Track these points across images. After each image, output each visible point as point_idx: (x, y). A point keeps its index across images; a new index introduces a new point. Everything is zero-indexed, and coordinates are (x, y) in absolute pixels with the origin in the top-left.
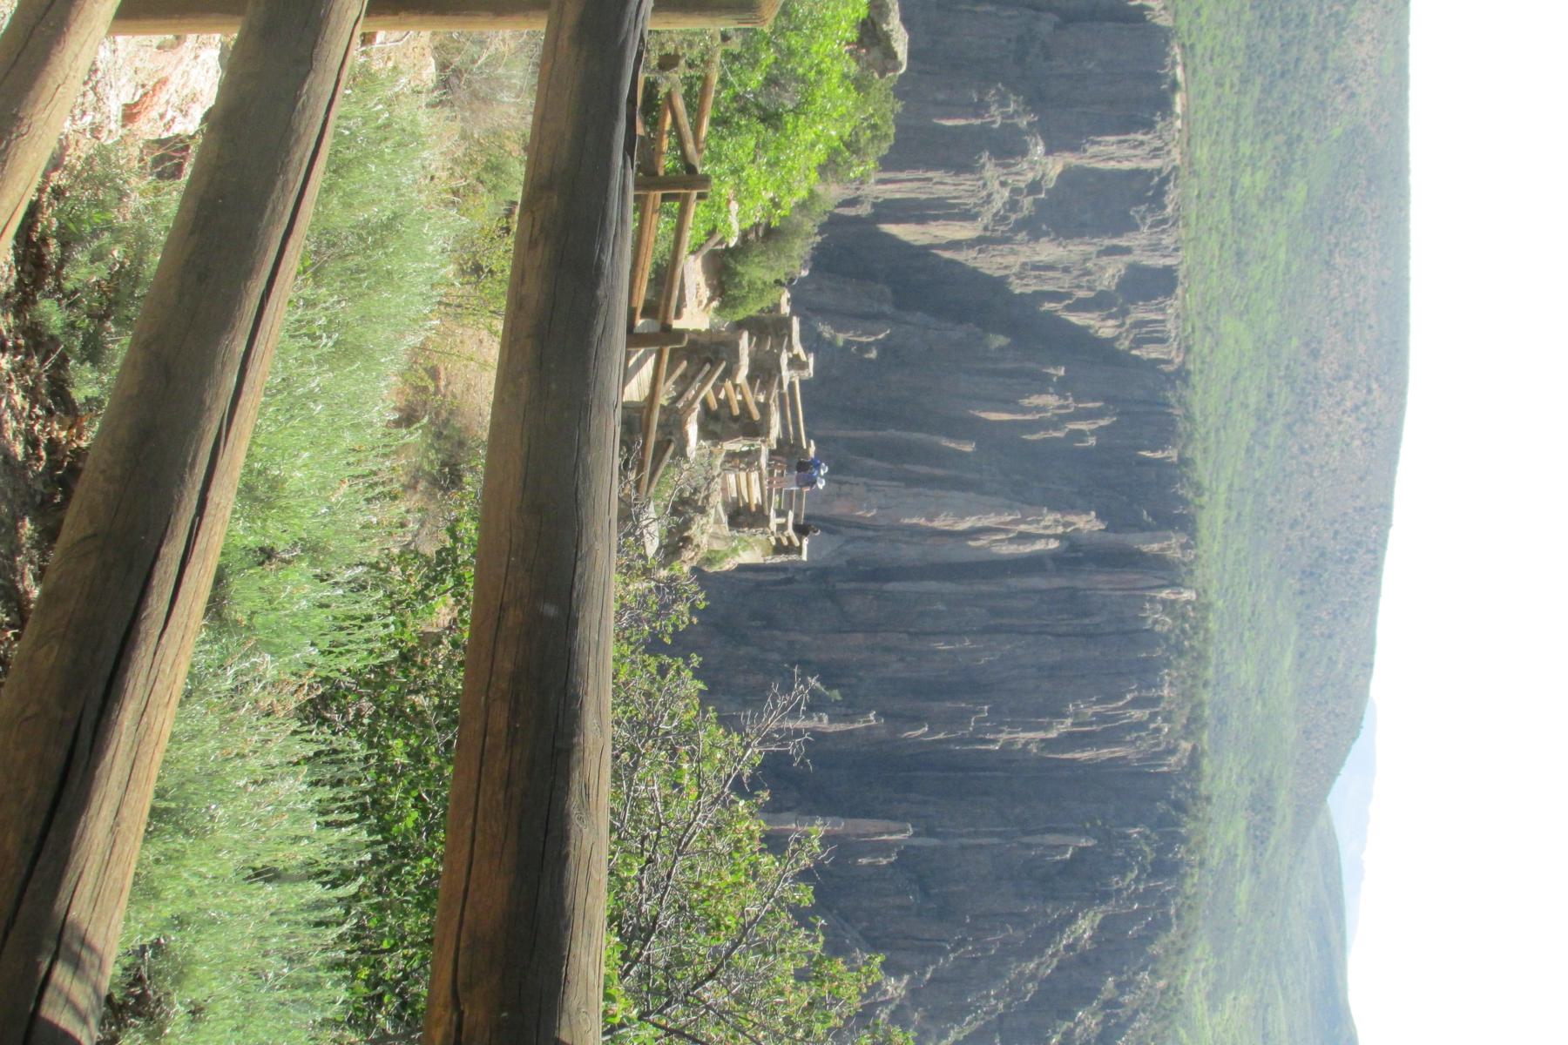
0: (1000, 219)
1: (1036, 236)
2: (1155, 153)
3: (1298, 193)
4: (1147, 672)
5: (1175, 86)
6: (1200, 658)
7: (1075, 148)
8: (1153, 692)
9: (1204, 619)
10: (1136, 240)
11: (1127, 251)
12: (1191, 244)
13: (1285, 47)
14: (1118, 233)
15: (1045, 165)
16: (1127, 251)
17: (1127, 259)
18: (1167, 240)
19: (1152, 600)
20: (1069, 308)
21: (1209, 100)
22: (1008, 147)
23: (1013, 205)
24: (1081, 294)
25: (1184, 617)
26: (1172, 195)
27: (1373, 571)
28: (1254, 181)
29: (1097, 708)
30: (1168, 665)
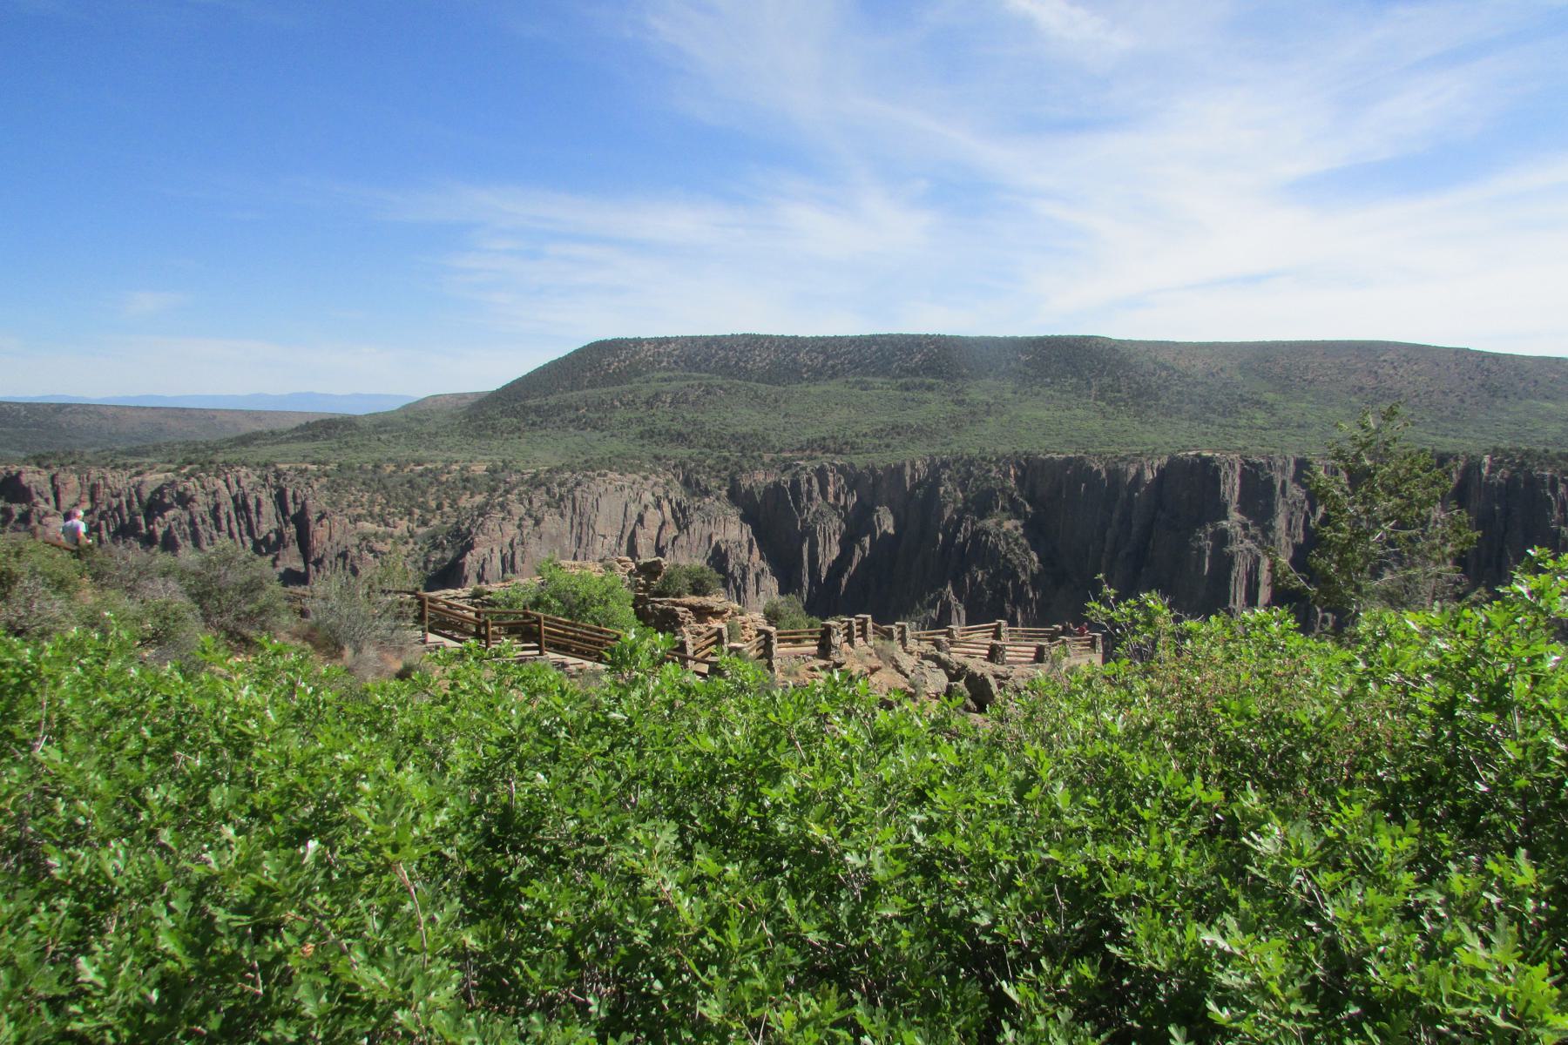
0: (1261, 545)
1: (1271, 528)
2: (1232, 466)
3: (1270, 397)
4: (1534, 483)
5: (1198, 456)
6: (1527, 454)
7: (1226, 506)
8: (1547, 481)
9: (1503, 451)
10: (1278, 479)
11: (1284, 483)
12: (1283, 451)
13: (1192, 401)
14: (1274, 487)
15: (1234, 520)
16: (1284, 483)
17: (1289, 483)
18: (1280, 463)
19: (1488, 478)
20: (1314, 513)
21: (1213, 439)
22: (1222, 538)
23: (1254, 538)
24: (1306, 507)
25: (1501, 461)
26: (1256, 459)
27: (1496, 358)
28: (1260, 418)
29: (1556, 512)
30: (1530, 472)
